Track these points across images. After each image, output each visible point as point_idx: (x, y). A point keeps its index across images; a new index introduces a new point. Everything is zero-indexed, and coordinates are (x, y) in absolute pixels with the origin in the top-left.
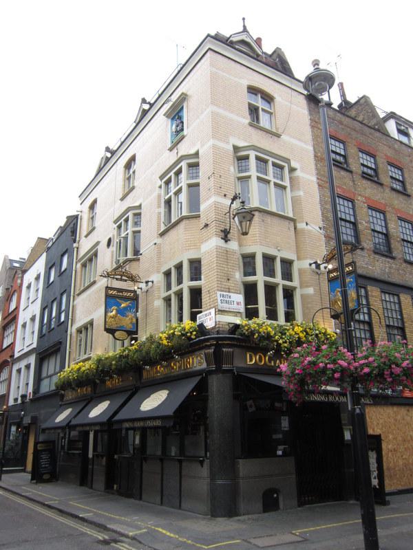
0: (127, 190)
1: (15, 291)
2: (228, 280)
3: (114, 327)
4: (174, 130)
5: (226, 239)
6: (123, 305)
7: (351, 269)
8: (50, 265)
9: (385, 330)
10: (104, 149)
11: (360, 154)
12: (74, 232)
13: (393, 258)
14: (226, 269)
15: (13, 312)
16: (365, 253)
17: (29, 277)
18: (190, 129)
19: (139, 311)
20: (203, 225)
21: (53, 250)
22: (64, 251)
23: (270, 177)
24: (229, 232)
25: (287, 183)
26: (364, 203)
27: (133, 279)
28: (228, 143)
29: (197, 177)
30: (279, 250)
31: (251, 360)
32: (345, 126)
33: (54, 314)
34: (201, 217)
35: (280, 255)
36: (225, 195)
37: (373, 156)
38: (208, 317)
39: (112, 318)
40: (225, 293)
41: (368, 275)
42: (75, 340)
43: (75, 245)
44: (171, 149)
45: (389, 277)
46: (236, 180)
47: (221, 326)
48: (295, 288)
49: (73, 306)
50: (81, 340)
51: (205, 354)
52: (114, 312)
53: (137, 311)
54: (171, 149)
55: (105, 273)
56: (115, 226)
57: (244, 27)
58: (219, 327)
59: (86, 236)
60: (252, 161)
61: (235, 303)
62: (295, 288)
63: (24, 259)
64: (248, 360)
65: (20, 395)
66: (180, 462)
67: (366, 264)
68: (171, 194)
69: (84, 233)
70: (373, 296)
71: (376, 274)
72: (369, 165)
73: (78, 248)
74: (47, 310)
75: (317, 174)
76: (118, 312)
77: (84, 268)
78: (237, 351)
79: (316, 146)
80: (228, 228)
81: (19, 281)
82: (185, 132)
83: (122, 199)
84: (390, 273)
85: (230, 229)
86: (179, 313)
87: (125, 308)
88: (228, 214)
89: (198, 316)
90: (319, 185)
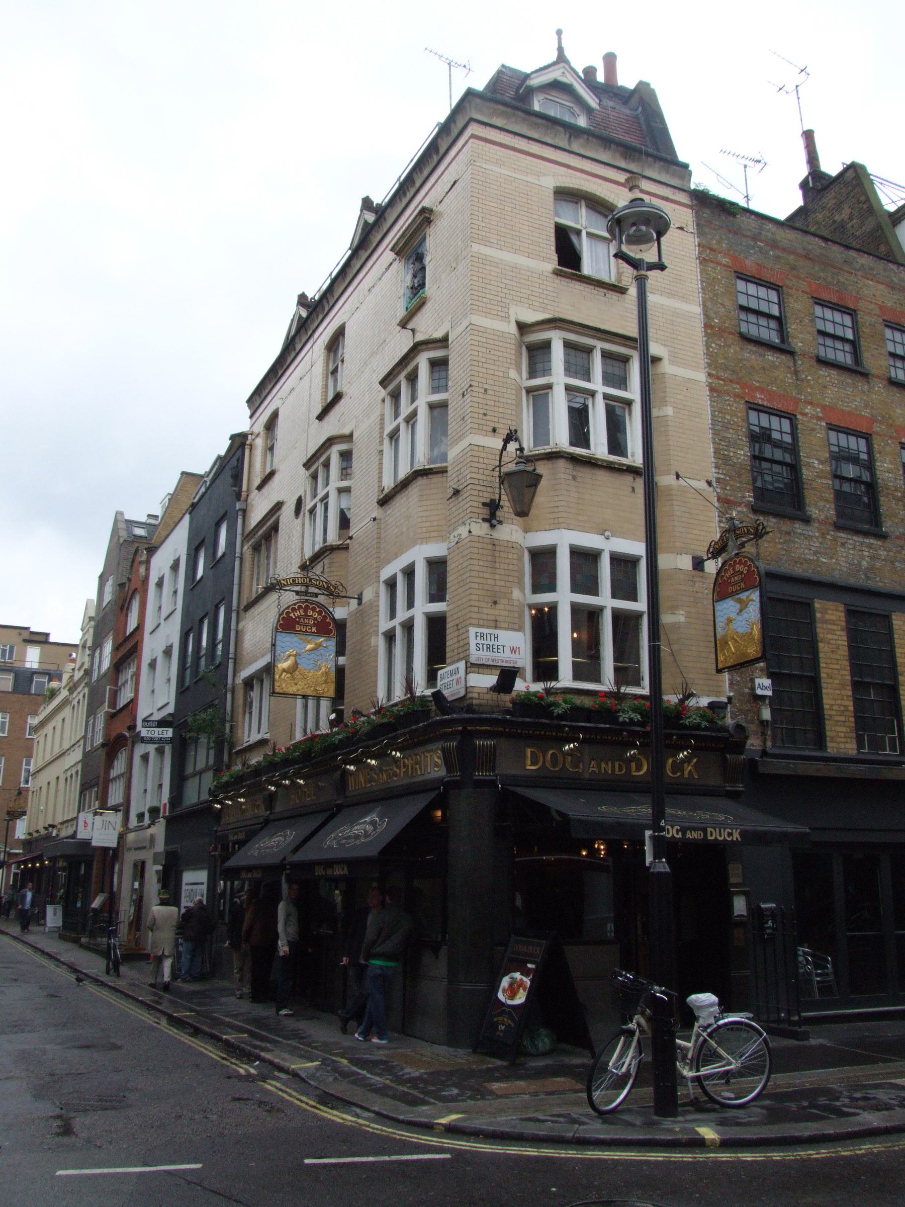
1: (135, 590)
2: (495, 603)
8: (197, 543)
9: (850, 693)
10: (359, 204)
11: (818, 311)
12: (237, 477)
13: (883, 537)
14: (490, 582)
15: (132, 633)
16: (813, 531)
17: (161, 563)
20: (450, 492)
21: (202, 511)
22: (221, 514)
26: (819, 419)
28: (507, 318)
29: (446, 388)
30: (607, 538)
32: (784, 250)
33: (204, 643)
34: (449, 474)
37: (852, 313)
38: (454, 677)
40: (485, 631)
41: (816, 577)
43: (238, 506)
45: (868, 578)
46: (524, 393)
49: (237, 632)
56: (307, 473)
57: (560, 50)
59: (260, 488)
60: (558, 352)
63: (156, 517)
64: (529, 762)
65: (147, 807)
67: (815, 553)
69: (257, 481)
70: (826, 622)
71: (836, 573)
72: (839, 333)
73: (244, 511)
74: (206, 622)
75: (709, 365)
79: (709, 304)
80: (497, 496)
81: (142, 570)
83: (320, 417)
84: (872, 569)
89: (439, 673)
90: (712, 389)
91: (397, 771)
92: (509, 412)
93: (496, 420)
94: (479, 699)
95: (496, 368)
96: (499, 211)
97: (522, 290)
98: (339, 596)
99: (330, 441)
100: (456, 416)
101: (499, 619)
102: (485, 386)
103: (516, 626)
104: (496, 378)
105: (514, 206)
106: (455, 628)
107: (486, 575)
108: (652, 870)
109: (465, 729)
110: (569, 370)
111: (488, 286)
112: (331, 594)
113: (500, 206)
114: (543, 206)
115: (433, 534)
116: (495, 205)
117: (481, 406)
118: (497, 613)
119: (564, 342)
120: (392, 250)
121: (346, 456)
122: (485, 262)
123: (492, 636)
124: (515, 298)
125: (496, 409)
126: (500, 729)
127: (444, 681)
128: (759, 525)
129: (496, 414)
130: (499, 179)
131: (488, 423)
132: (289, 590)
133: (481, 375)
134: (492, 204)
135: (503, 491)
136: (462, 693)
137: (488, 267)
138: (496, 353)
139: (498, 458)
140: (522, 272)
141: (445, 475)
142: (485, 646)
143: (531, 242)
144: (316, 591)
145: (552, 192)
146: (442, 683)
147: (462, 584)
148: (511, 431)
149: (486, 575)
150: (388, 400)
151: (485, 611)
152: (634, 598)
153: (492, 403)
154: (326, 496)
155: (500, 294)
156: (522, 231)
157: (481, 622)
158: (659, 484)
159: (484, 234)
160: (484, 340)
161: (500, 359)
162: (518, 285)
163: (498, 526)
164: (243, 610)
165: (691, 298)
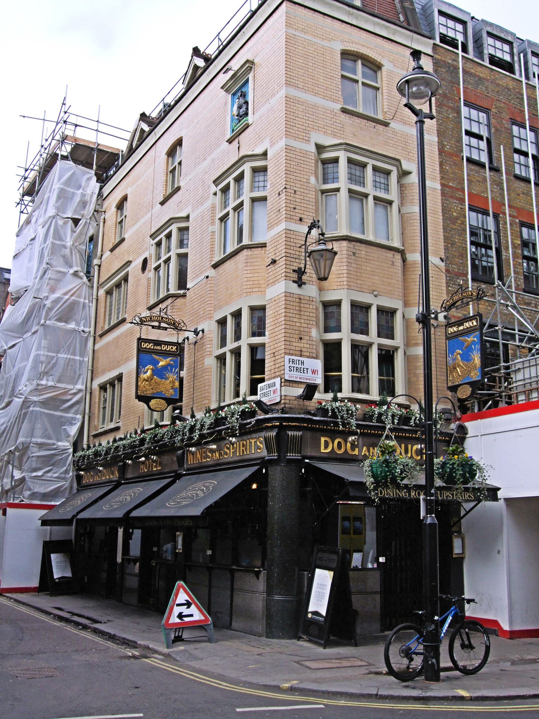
0: (169, 191)
2: (301, 339)
3: (149, 393)
4: (235, 112)
5: (300, 283)
6: (161, 364)
7: (475, 323)
10: (191, 51)
14: (298, 324)
18: (257, 115)
19: (185, 369)
20: (269, 261)
23: (369, 189)
24: (304, 273)
25: (393, 195)
27: (176, 326)
30: (376, 296)
31: (326, 447)
34: (267, 248)
35: (375, 302)
36: (301, 220)
38: (272, 389)
39: (147, 381)
42: (97, 400)
44: (230, 141)
46: (320, 193)
47: (288, 401)
48: (396, 349)
50: (105, 401)
51: (265, 439)
52: (149, 373)
53: (181, 369)
54: (230, 141)
55: (137, 319)
58: (285, 403)
60: (343, 164)
61: (309, 371)
62: (396, 349)
66: (232, 572)
68: (229, 208)
73: (99, 266)
76: (155, 372)
77: (109, 297)
78: (308, 434)
80: (303, 266)
82: (250, 119)
83: (162, 203)
85: (305, 268)
86: (235, 379)
87: (165, 368)
88: (304, 247)
91: (228, 451)
92: (311, 207)
93: (302, 212)
94: (289, 404)
95: (302, 176)
96: (304, 65)
97: (320, 122)
98: (181, 330)
99: (172, 221)
100: (274, 208)
101: (303, 349)
102: (295, 189)
103: (314, 355)
104: (302, 183)
105: (314, 62)
106: (272, 355)
107: (295, 320)
108: (424, 522)
109: (281, 424)
110: (351, 179)
111: (297, 119)
112: (177, 329)
113: (304, 62)
114: (334, 63)
115: (254, 290)
116: (301, 61)
117: (292, 202)
118: (302, 345)
119: (348, 159)
120: (226, 88)
121: (183, 230)
122: (294, 101)
123: (300, 362)
124: (315, 127)
125: (302, 205)
126: (305, 425)
127: (263, 391)
128: (479, 290)
129: (302, 208)
130: (304, 43)
131: (297, 215)
132: (148, 325)
133: (292, 181)
134: (299, 60)
135: (308, 263)
136: (278, 400)
137: (297, 105)
138: (302, 165)
139: (304, 239)
140: (319, 109)
141: (264, 249)
142: (295, 368)
143: (325, 88)
144: (166, 326)
145: (339, 53)
146: (261, 392)
147: (278, 325)
148: (314, 221)
149: (295, 320)
150: (219, 193)
151: (294, 344)
152: (391, 337)
153: (299, 201)
154: (169, 259)
155: (305, 124)
156: (319, 80)
157: (291, 352)
158: (408, 260)
159: (294, 81)
160: (294, 156)
161: (305, 170)
162: (317, 118)
163: (303, 286)
164: (99, 336)
165: (432, 131)
